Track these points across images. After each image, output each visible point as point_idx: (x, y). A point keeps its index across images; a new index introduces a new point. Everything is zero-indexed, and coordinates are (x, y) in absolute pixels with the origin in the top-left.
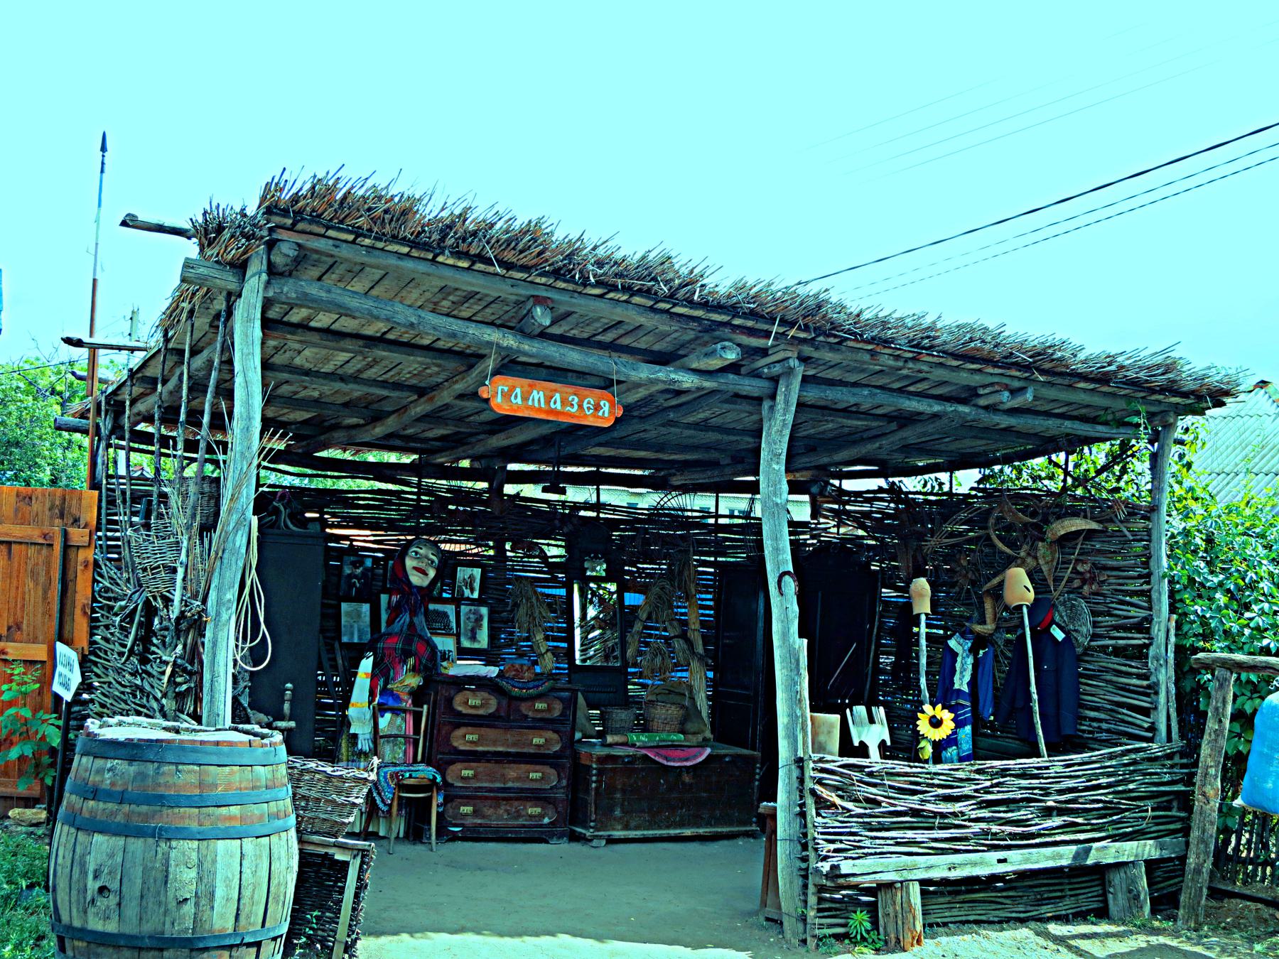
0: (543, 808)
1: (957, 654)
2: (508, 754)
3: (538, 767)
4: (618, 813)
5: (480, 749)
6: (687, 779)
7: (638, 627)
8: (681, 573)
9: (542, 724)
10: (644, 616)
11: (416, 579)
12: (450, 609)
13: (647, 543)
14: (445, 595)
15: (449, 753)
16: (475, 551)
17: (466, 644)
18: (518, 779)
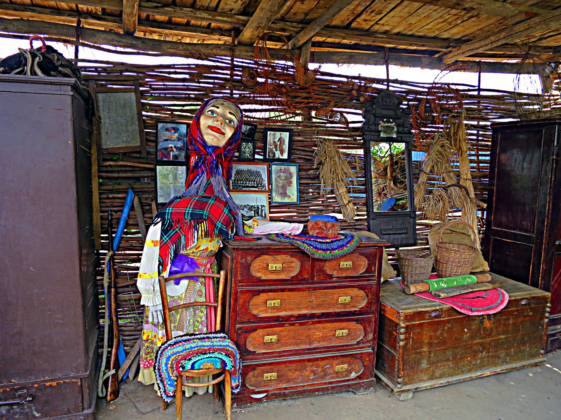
0: (350, 365)
2: (313, 316)
3: (344, 324)
4: (424, 364)
5: (282, 314)
6: (487, 324)
7: (423, 178)
8: (456, 133)
9: (349, 282)
10: (428, 170)
11: (210, 138)
12: (262, 169)
13: (429, 110)
14: (257, 156)
15: (249, 322)
16: (283, 117)
17: (277, 199)
18: (324, 338)
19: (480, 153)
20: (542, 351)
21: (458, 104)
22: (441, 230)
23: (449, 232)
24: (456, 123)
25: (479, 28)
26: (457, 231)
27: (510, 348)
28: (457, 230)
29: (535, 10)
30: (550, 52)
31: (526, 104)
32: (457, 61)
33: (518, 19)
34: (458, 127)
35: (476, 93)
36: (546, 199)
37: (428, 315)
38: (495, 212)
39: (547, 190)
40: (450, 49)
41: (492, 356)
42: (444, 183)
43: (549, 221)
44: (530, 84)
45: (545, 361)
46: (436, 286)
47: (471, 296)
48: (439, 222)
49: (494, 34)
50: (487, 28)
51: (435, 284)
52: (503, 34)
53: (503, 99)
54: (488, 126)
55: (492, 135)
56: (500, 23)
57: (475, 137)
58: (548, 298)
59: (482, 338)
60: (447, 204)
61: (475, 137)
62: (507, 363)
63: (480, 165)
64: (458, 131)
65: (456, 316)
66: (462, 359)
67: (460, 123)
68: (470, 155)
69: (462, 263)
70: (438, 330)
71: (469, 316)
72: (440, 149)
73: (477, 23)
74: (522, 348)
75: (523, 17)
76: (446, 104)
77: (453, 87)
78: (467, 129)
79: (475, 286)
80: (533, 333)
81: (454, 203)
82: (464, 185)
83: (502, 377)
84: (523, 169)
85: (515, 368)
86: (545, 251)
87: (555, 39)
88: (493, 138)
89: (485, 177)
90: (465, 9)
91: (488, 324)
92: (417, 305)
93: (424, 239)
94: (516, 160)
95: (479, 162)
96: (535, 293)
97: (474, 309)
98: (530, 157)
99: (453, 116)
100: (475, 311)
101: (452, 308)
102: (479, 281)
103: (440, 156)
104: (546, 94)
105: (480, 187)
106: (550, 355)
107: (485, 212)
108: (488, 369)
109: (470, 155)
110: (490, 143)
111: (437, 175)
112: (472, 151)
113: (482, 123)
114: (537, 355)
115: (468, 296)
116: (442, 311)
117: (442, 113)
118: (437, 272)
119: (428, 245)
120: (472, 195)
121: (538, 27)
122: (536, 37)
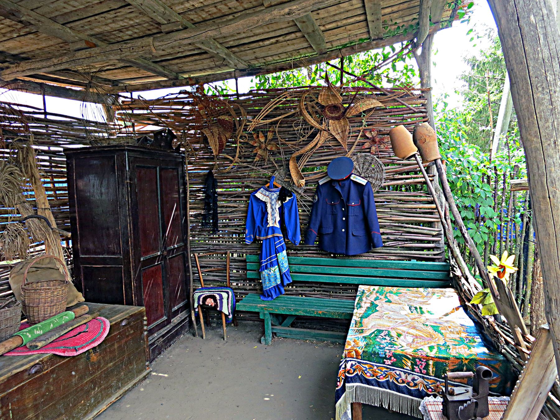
1: (265, 203)
8: (25, 159)
19: (55, 180)
20: (147, 363)
21: (23, 127)
22: (23, 269)
23: (34, 269)
24: (24, 147)
25: (39, 47)
26: (44, 267)
27: (120, 372)
28: (43, 266)
29: (94, 41)
30: (109, 84)
31: (96, 131)
32: (16, 80)
33: (79, 46)
34: (27, 153)
35: (42, 116)
36: (126, 221)
37: (27, 373)
38: (80, 239)
39: (126, 212)
40: (6, 64)
41: (105, 389)
42: (20, 215)
43: (132, 241)
44: (94, 112)
45: (151, 371)
46: (30, 336)
47: (72, 334)
48: (19, 260)
49: (56, 57)
50: (47, 49)
51: (28, 334)
52: (65, 59)
53: (69, 125)
54: (60, 152)
55: (66, 161)
56: (61, 47)
57: (48, 164)
58: (143, 312)
59: (91, 375)
60: (26, 239)
61: (48, 164)
62: (119, 388)
63: (58, 192)
64: (27, 156)
65: (59, 362)
66: (75, 406)
67: (29, 149)
68: (45, 183)
69: (55, 302)
70: (41, 387)
71: (74, 357)
72: (9, 177)
73: (36, 42)
74: (130, 367)
75: (84, 45)
76: (10, 126)
77: (15, 107)
78: (38, 155)
79: (75, 322)
80: (137, 349)
81: (34, 237)
82: (43, 215)
83: (117, 405)
84: (101, 194)
85: (128, 390)
86: (133, 269)
87: (113, 73)
88: (68, 164)
89: (64, 204)
90: (21, 22)
91: (95, 357)
92: (11, 367)
93: (4, 284)
94: (94, 186)
95: (55, 189)
96: (132, 311)
97: (78, 347)
98: (106, 182)
99: (20, 140)
100: (79, 349)
101: (54, 355)
102: (77, 316)
103: (9, 185)
104: (111, 123)
105: (60, 216)
106: (154, 363)
107: (70, 241)
108: (103, 403)
109: (45, 183)
110: (65, 170)
111: (9, 207)
112: (47, 178)
113: (53, 149)
114: (144, 369)
115: (69, 336)
116: (43, 363)
117: (6, 136)
118: (29, 319)
119: (11, 290)
120: (54, 225)
121: (99, 58)
122: (96, 68)
